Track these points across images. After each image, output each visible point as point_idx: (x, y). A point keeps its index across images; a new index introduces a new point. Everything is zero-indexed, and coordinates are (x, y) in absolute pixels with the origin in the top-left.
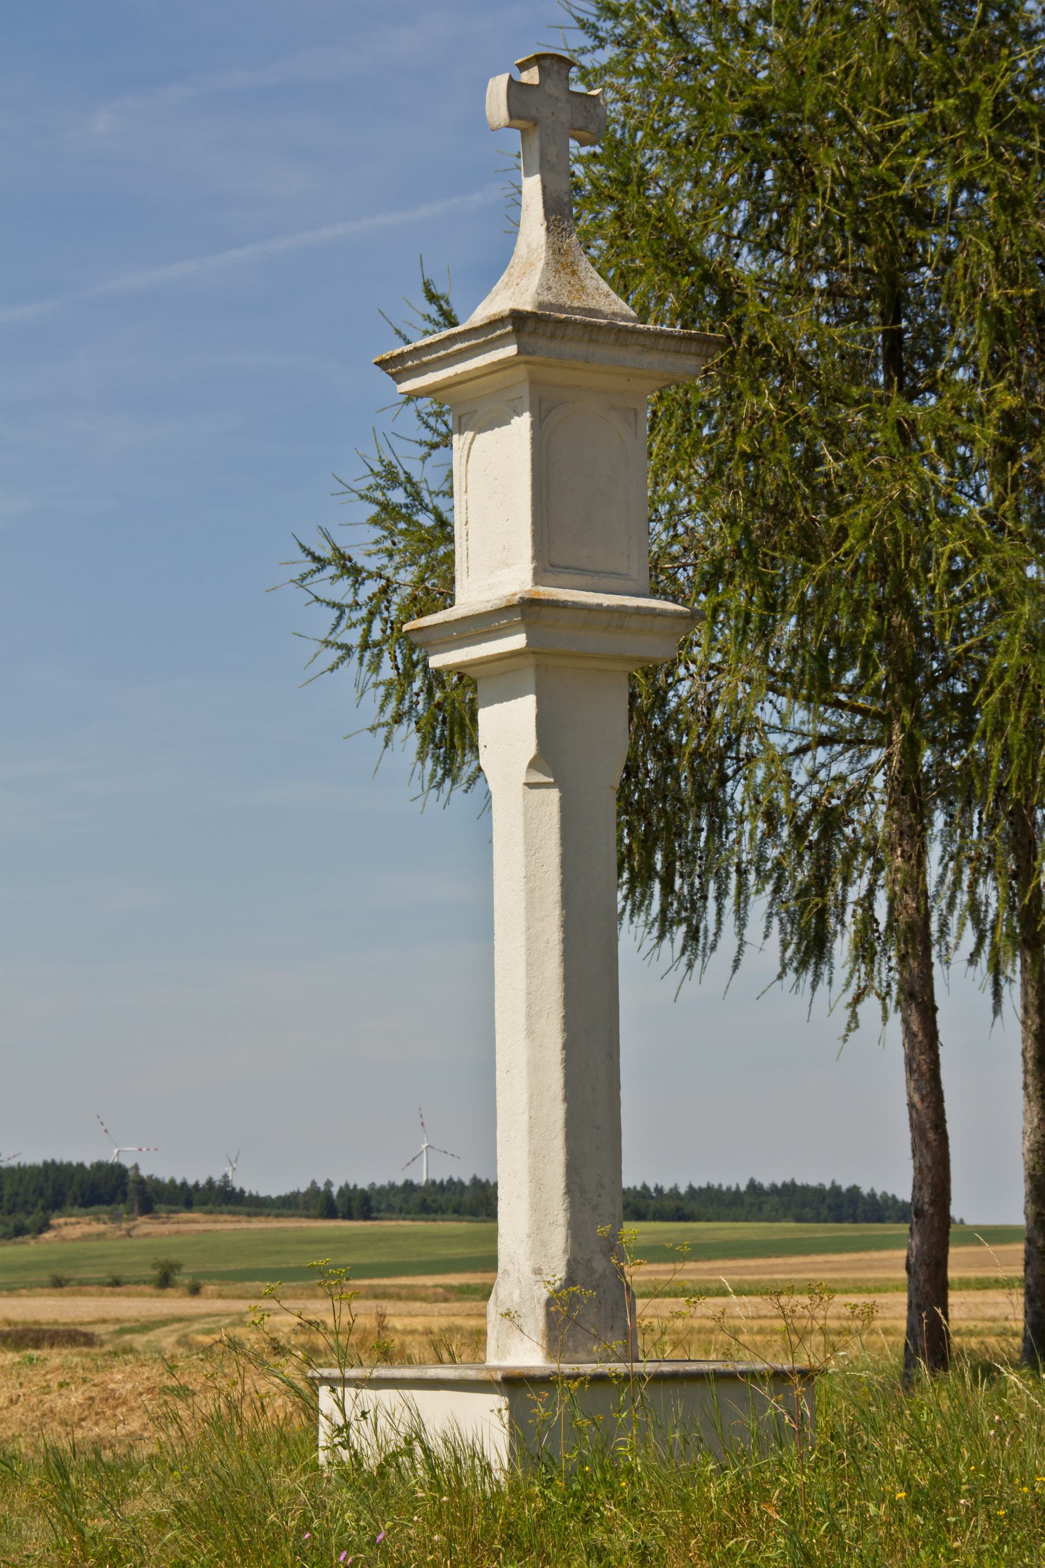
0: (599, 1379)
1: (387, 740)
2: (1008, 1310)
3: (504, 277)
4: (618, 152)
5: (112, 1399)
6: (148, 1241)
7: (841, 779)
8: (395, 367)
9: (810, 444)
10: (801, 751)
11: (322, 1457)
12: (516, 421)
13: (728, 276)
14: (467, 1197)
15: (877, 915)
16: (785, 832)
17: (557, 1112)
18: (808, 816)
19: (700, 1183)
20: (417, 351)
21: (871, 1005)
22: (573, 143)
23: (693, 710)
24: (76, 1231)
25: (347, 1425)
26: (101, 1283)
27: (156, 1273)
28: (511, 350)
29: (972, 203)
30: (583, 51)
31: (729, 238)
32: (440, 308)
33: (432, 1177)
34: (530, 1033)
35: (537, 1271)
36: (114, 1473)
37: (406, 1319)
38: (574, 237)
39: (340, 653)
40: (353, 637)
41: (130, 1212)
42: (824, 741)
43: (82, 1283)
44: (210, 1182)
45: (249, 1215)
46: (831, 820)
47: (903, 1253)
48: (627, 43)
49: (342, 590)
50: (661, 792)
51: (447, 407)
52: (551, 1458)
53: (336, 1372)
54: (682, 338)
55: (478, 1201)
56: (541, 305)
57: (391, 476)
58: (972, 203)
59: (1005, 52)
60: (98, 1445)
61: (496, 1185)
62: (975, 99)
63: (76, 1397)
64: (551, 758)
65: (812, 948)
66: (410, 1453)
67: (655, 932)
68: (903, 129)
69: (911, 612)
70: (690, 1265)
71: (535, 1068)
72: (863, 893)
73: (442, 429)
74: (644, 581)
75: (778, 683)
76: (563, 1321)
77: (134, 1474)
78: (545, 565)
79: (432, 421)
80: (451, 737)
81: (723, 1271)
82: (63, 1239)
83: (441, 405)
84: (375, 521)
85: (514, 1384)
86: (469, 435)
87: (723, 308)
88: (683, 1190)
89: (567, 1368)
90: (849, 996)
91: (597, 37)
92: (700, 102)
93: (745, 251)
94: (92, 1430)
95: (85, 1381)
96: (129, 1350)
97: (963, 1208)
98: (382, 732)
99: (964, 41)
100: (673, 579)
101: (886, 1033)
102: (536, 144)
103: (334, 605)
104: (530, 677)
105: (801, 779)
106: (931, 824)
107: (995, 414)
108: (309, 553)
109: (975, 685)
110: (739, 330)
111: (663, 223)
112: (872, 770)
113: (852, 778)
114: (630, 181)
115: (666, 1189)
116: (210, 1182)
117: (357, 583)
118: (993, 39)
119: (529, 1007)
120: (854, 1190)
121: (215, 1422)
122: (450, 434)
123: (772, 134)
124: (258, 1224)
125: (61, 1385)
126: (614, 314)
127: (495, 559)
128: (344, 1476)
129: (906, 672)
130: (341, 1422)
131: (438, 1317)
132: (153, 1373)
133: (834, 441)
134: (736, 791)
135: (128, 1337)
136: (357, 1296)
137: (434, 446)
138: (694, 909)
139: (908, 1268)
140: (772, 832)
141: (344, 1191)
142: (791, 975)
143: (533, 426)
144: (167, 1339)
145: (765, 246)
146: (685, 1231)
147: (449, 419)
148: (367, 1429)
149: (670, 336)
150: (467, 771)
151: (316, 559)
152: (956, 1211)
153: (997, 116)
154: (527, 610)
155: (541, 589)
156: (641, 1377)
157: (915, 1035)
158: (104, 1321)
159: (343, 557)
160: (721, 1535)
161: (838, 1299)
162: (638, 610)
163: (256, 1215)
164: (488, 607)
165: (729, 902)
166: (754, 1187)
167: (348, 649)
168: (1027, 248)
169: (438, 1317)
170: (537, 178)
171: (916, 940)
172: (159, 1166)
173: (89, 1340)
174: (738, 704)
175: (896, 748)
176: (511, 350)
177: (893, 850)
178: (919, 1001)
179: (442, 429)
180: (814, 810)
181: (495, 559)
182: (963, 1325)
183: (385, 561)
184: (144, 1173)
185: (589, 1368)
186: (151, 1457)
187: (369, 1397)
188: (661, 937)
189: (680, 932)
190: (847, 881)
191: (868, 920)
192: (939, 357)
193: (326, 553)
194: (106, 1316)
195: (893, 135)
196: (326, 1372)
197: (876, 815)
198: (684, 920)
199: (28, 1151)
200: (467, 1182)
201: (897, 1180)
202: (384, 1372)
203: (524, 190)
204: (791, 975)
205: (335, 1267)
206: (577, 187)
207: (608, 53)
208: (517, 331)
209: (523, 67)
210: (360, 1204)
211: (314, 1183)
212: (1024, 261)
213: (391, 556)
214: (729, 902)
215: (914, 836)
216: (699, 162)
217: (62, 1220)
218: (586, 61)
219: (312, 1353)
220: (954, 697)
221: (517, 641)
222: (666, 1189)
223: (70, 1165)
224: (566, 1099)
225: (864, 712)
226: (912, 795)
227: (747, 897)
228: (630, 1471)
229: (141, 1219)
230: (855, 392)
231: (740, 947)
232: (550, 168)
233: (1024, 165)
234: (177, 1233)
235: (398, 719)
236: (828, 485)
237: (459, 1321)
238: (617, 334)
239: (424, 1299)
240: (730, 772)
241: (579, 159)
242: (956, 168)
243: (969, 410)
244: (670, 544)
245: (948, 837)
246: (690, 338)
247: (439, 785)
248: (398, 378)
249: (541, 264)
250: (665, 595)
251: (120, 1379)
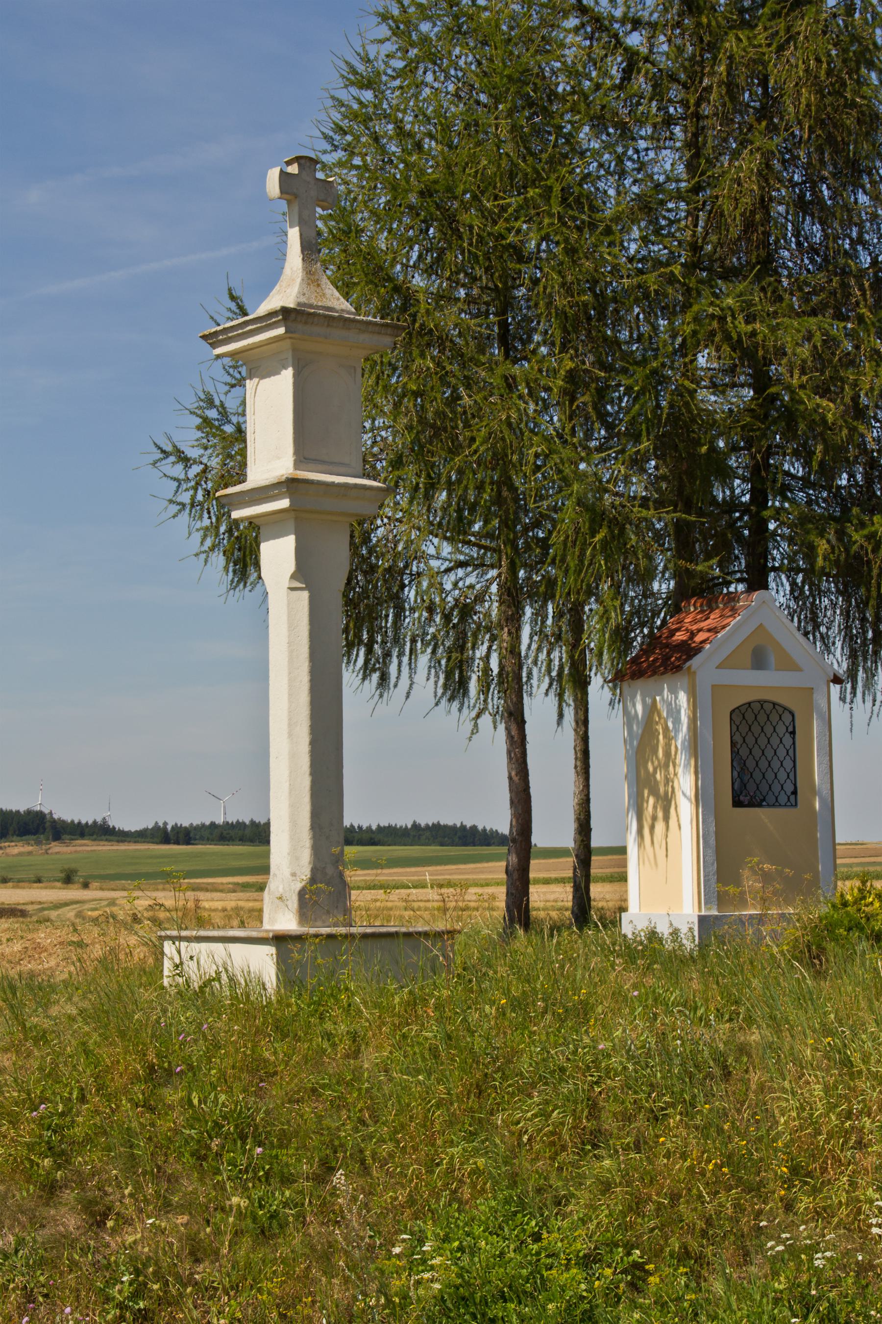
0: (330, 936)
1: (206, 561)
2: (563, 896)
3: (277, 287)
4: (343, 215)
5: (39, 948)
6: (58, 856)
7: (471, 587)
8: (212, 339)
9: (455, 389)
10: (448, 570)
11: (166, 982)
12: (284, 372)
13: (408, 288)
14: (247, 832)
15: (492, 666)
16: (438, 619)
17: (306, 782)
18: (452, 609)
19: (384, 823)
20: (226, 330)
21: (486, 720)
22: (319, 210)
23: (385, 545)
24: (16, 851)
25: (182, 963)
26: (30, 881)
27: (63, 875)
28: (281, 331)
29: (549, 251)
30: (325, 152)
31: (407, 267)
32: (238, 304)
34: (290, 735)
35: (294, 875)
36: (42, 990)
37: (211, 902)
38: (319, 264)
39: (178, 507)
40: (186, 498)
41: (48, 839)
42: (461, 564)
43: (20, 881)
44: (95, 822)
45: (118, 841)
46: (466, 611)
47: (504, 864)
48: (350, 150)
49: (178, 470)
50: (365, 594)
51: (240, 363)
52: (301, 982)
53: (175, 933)
54: (383, 325)
55: (258, 834)
57: (210, 402)
58: (549, 251)
59: (568, 161)
60: (32, 975)
61: (268, 824)
62: (550, 189)
63: (17, 947)
64: (305, 572)
65: (455, 687)
66: (219, 979)
67: (360, 676)
68: (509, 205)
69: (513, 489)
70: (386, 871)
71: (293, 756)
72: (484, 654)
73: (238, 376)
74: (358, 466)
75: (435, 529)
76: (308, 903)
77: (54, 991)
78: (302, 457)
79: (231, 371)
80: (243, 559)
81: (427, 874)
82: (7, 855)
83: (237, 362)
84: (199, 428)
85: (280, 940)
86: (256, 380)
87: (404, 309)
88: (374, 827)
89: (312, 931)
90: (474, 714)
91: (333, 145)
92: (393, 187)
93: (416, 275)
94: (28, 966)
95: (22, 938)
96: (48, 920)
97: (539, 838)
98: (203, 556)
99: (544, 156)
100: (374, 467)
101: (494, 738)
102: (296, 209)
103: (175, 479)
104: (291, 525)
105: (448, 586)
106: (524, 614)
107: (563, 372)
108: (159, 448)
109: (550, 533)
110: (414, 321)
111: (370, 256)
112: (490, 582)
113: (478, 587)
114: (348, 232)
115: (364, 828)
116: (95, 822)
117: (187, 467)
118: (561, 154)
119: (290, 719)
120: (474, 827)
121: (102, 961)
122: (244, 379)
123: (435, 207)
124: (123, 847)
125: (8, 940)
126: (342, 310)
127: (271, 454)
128: (180, 993)
129: (508, 524)
130: (177, 961)
131: (231, 901)
132: (65, 934)
133: (468, 387)
134: (410, 594)
135: (46, 912)
136: (187, 889)
137: (233, 386)
138: (384, 662)
139: (507, 872)
140: (430, 619)
141: (175, 827)
142: (444, 701)
143: (294, 376)
144: (70, 913)
145: (429, 271)
146: (375, 852)
147: (244, 370)
148: (193, 965)
149: (376, 324)
150: (253, 577)
151: (163, 452)
152: (535, 839)
153: (564, 200)
154: (290, 485)
155: (298, 472)
156: (353, 936)
157: (512, 737)
158: (32, 903)
159: (179, 451)
160: (399, 1027)
161: (472, 890)
162: (356, 486)
163: (123, 841)
164: (267, 483)
165: (405, 659)
166: (415, 826)
167: (183, 505)
168: (581, 277)
169: (231, 901)
170: (297, 229)
171: (512, 684)
172: (66, 812)
173: (23, 914)
174: (412, 542)
175: (504, 569)
176: (281, 331)
177: (502, 629)
178: (515, 718)
179: (238, 376)
180: (456, 605)
181: (271, 454)
182: (541, 905)
183: (202, 451)
184: (56, 817)
185: (325, 931)
186: (63, 981)
187: (196, 947)
188: (364, 679)
189: (376, 676)
190: (473, 648)
191: (487, 670)
192: (530, 340)
193: (169, 448)
194: (33, 900)
195: (503, 209)
196: (168, 933)
197: (493, 608)
198: (378, 670)
199: (17, 801)
200: (247, 822)
201: (501, 821)
202: (202, 933)
203: (289, 235)
204: (444, 701)
205: (177, 872)
206: (319, 234)
207: (340, 154)
208: (285, 319)
209: (289, 163)
210: (184, 836)
211: (156, 823)
212: (579, 284)
213: (206, 448)
214: (405, 659)
215: (513, 620)
216: (392, 220)
217: (7, 844)
218: (325, 158)
219: (157, 922)
220: (539, 540)
221: (284, 503)
222: (364, 828)
223: (11, 811)
224: (311, 774)
225: (486, 548)
226: (513, 597)
227: (416, 656)
228: (347, 989)
229: (53, 844)
230: (483, 359)
231: (411, 685)
232: (304, 223)
233: (579, 229)
234: (76, 852)
235: (212, 549)
236: (465, 412)
237: (241, 904)
238: (344, 322)
239: (221, 891)
240: (406, 582)
241: (321, 218)
242: (540, 229)
243: (547, 371)
244: (372, 447)
245: (534, 622)
246: (387, 325)
247: (235, 589)
248: (214, 346)
249: (299, 280)
250: (368, 477)
251: (42, 936)
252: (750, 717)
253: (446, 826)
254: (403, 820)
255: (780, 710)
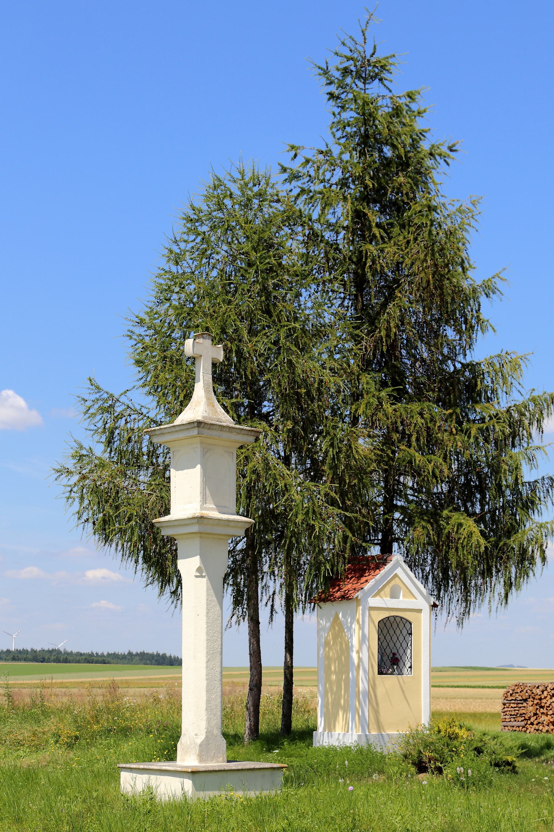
33: (16, 648)
56: (203, 417)
74: (234, 508)
88: (105, 654)
120: (164, 655)
164: (185, 517)
166: (130, 654)
200: (29, 650)
202: (128, 766)
238: (222, 428)
249: (203, 403)
252: (388, 625)
253: (147, 654)
254: (123, 650)
255: (404, 621)
